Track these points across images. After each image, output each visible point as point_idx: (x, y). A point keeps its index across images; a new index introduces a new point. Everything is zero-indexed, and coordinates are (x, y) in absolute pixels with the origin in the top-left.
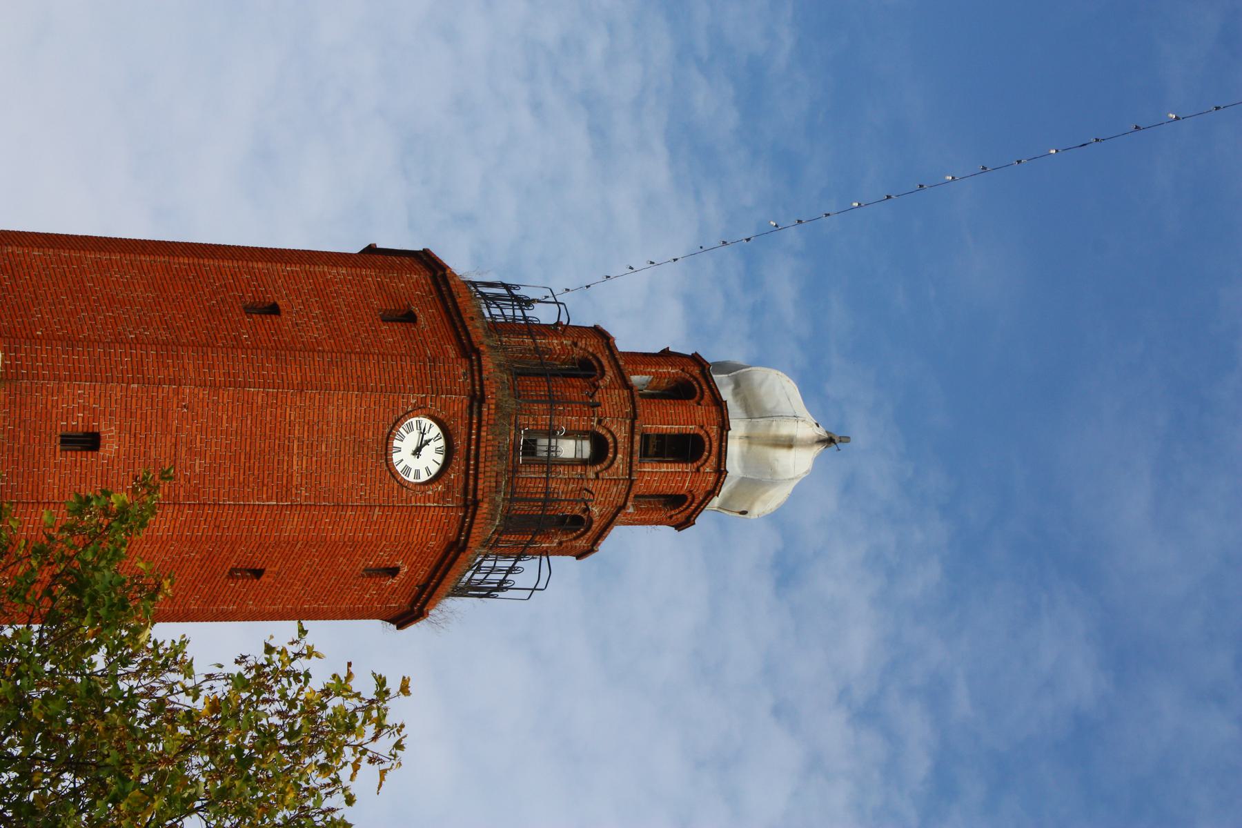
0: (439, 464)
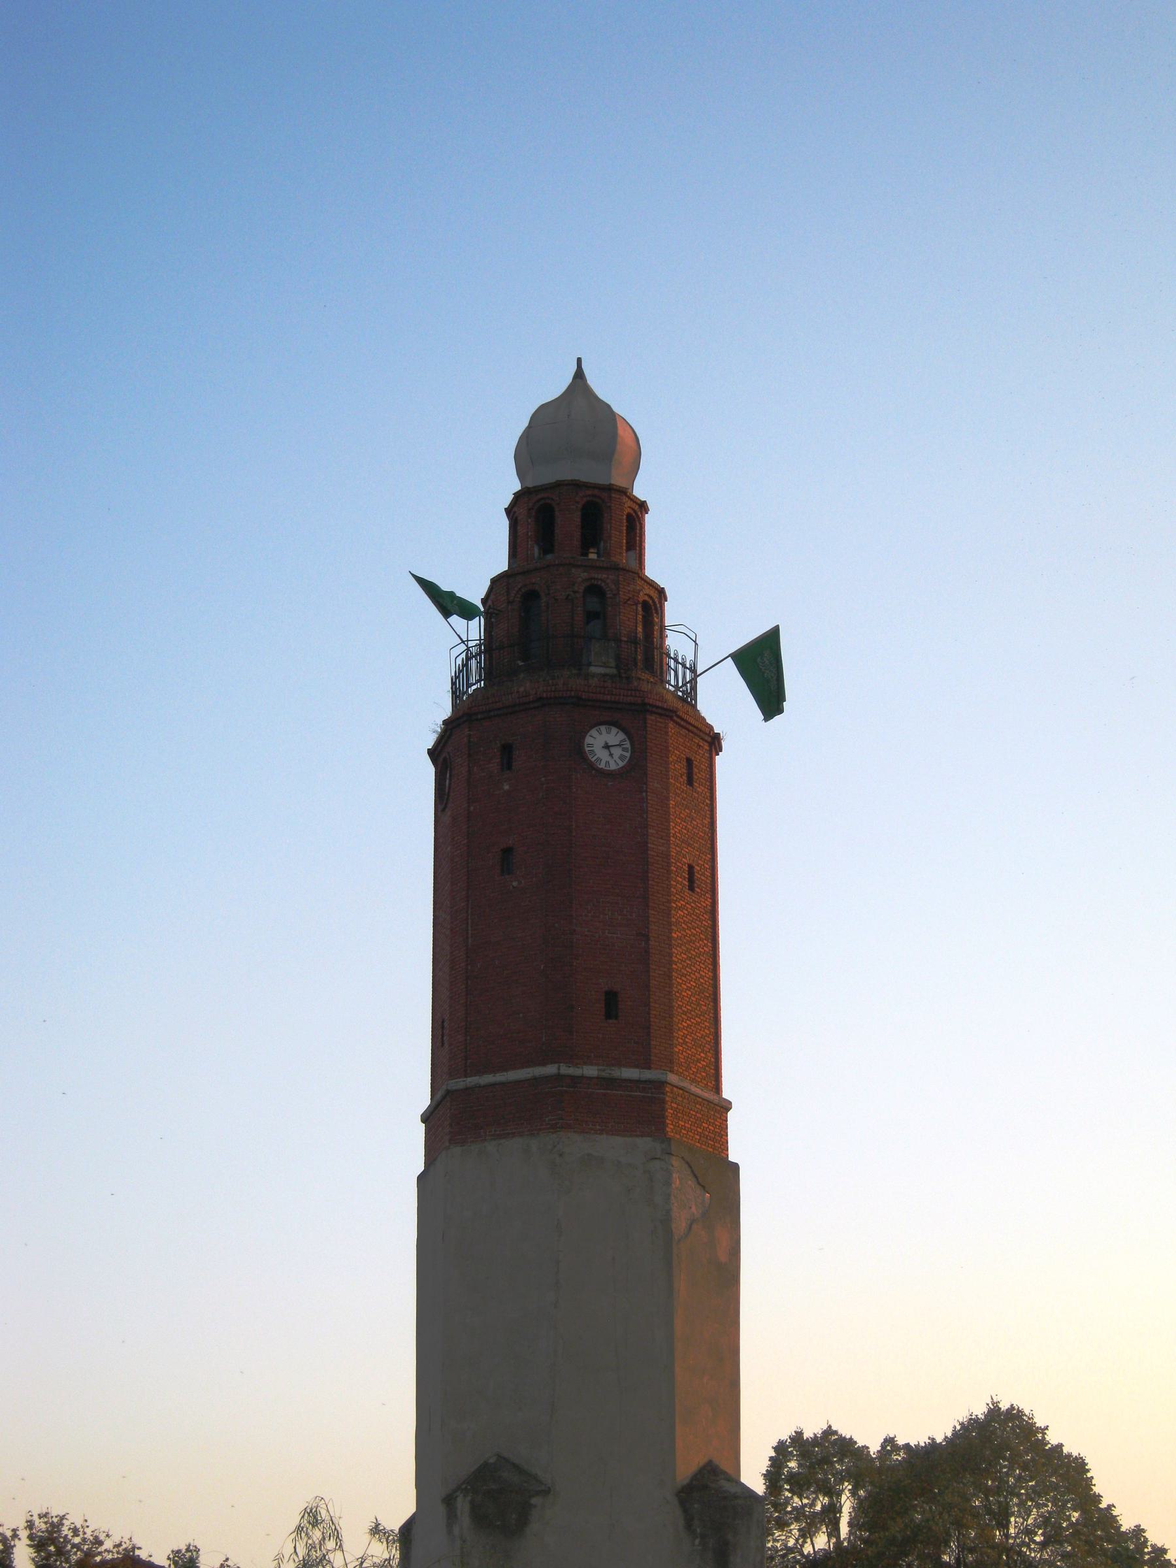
0: (618, 732)
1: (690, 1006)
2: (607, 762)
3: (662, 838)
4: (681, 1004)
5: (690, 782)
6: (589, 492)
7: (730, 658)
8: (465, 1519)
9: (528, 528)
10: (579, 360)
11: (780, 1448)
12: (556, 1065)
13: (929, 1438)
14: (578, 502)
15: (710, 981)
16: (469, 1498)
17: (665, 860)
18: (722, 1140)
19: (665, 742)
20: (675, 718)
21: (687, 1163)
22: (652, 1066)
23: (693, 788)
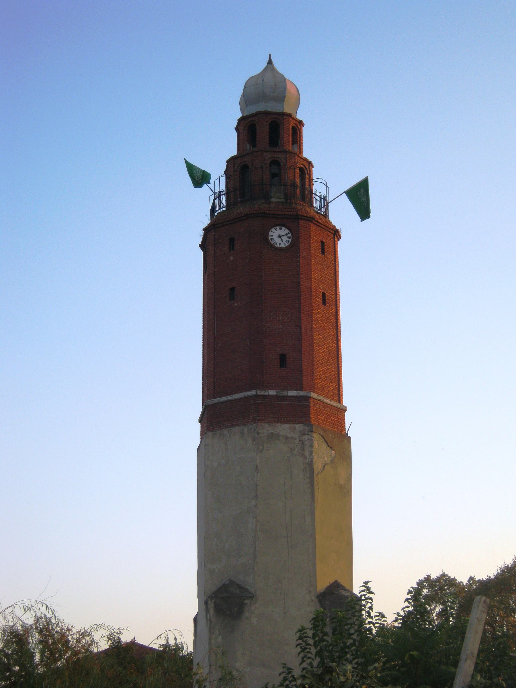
0: (285, 229)
1: (324, 360)
2: (280, 244)
3: (307, 280)
4: (319, 359)
5: (323, 252)
6: (273, 116)
7: (344, 193)
8: (212, 612)
9: (244, 136)
10: (270, 56)
11: (420, 584)
12: (255, 390)
13: (488, 576)
14: (267, 122)
15: (335, 349)
16: (213, 601)
17: (310, 290)
18: (342, 425)
19: (309, 233)
20: (314, 221)
21: (322, 436)
22: (303, 389)
23: (324, 255)
